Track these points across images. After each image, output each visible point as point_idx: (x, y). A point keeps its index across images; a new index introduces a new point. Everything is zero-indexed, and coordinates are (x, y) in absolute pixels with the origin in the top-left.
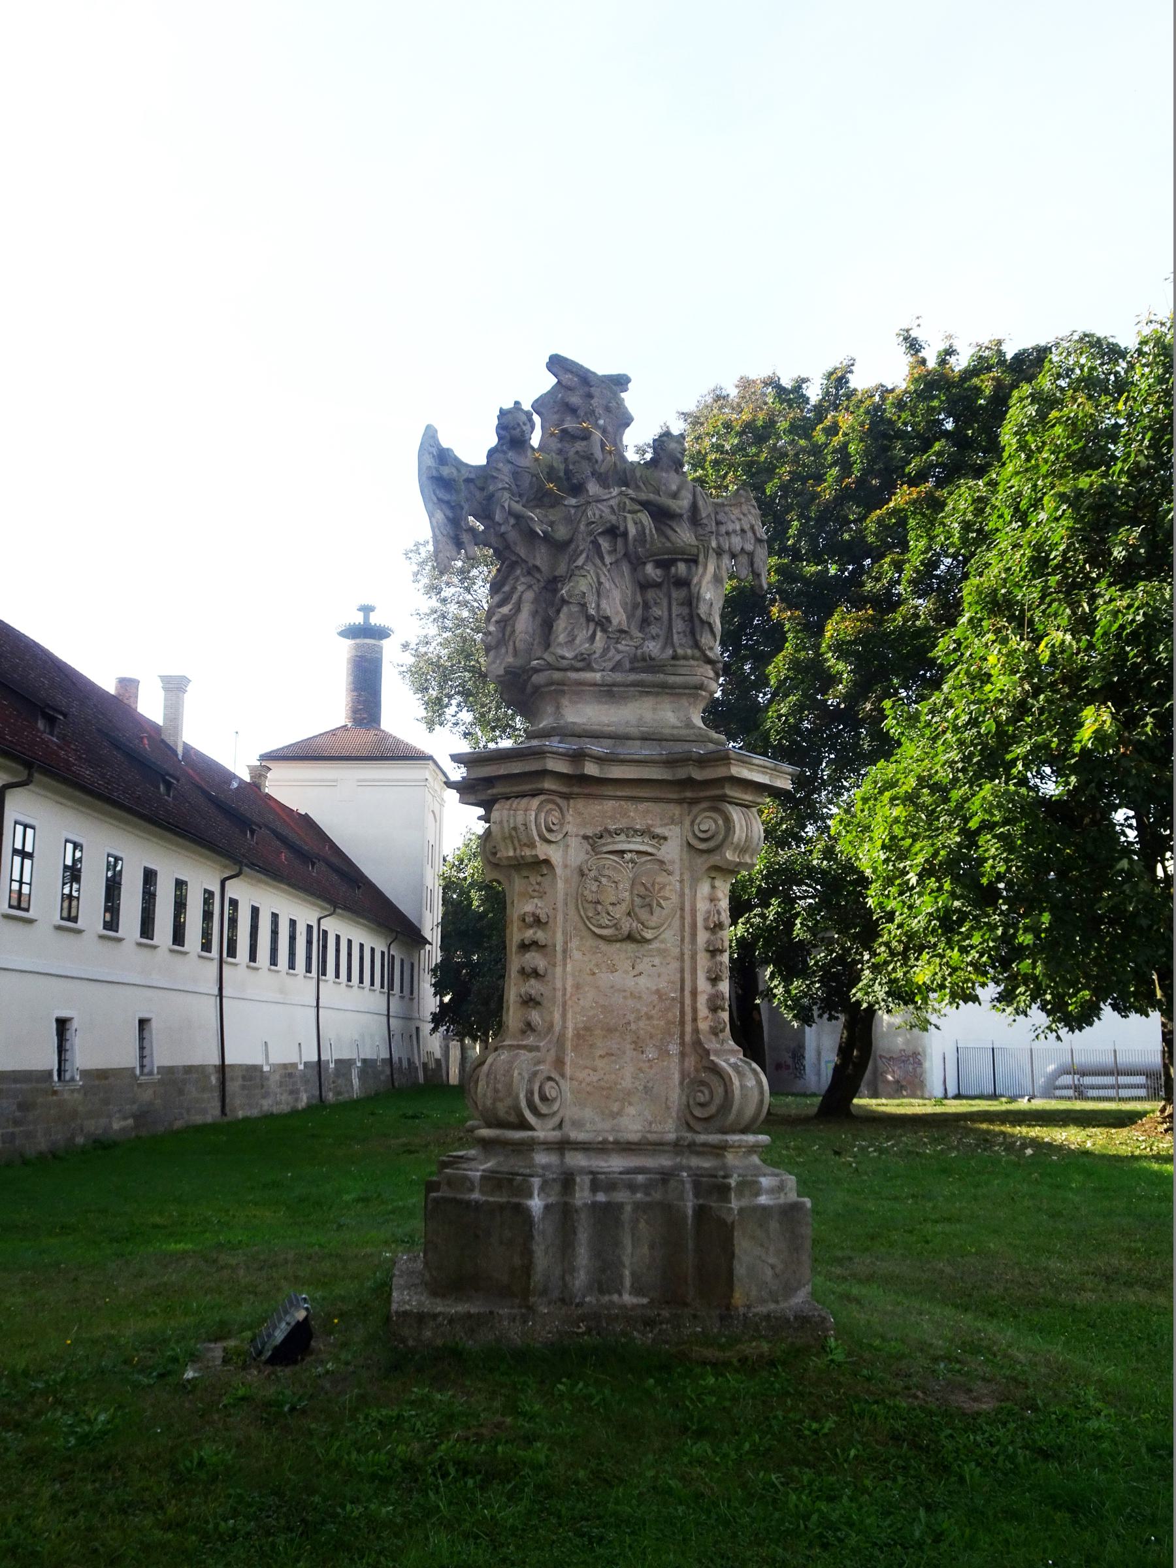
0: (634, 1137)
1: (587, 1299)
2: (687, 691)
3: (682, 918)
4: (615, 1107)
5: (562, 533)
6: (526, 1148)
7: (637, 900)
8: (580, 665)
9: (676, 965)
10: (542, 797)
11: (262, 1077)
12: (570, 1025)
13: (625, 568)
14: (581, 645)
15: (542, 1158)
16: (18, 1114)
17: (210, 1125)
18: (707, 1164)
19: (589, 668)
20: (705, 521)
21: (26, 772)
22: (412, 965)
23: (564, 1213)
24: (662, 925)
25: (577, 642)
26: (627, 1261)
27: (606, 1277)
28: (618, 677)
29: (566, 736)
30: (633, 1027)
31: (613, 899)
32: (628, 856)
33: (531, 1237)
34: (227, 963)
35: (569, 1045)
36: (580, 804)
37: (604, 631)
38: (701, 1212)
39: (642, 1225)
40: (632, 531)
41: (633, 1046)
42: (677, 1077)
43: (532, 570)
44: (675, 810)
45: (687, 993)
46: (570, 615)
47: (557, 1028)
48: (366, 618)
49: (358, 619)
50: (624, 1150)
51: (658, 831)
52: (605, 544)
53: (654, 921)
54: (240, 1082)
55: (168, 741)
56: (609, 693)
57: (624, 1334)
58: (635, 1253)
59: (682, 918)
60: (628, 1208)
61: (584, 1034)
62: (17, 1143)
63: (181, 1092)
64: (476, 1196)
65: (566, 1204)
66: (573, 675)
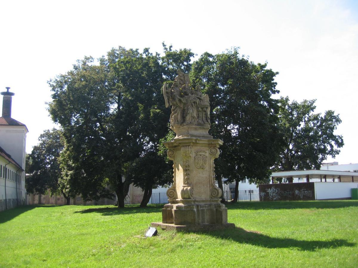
9: (208, 173)
18: (215, 203)
22: (20, 176)
30: (203, 182)
38: (216, 210)
42: (209, 190)
43: (180, 108)
48: (8, 90)
49: (6, 90)
52: (193, 104)
58: (207, 217)
60: (205, 210)
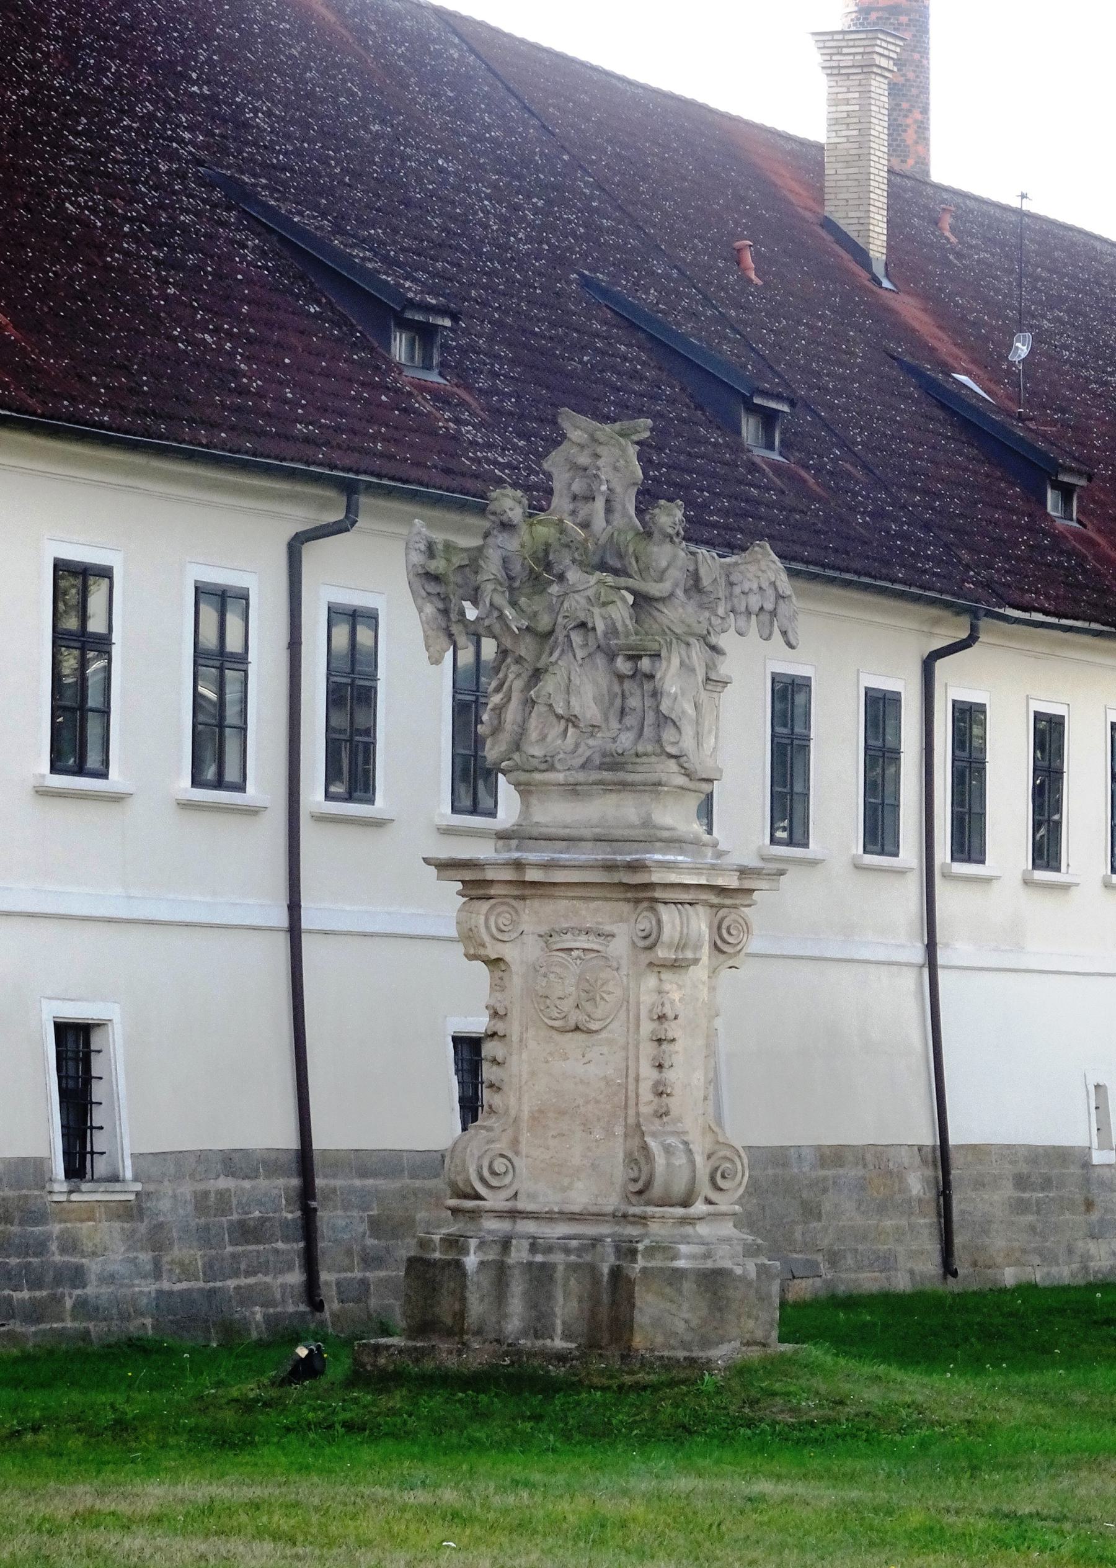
0: (576, 1209)
1: (522, 1342)
2: (647, 788)
3: (628, 1010)
4: (566, 1182)
5: (544, 623)
6: (474, 1215)
7: (583, 995)
8: (543, 766)
10: (492, 901)
11: (1087, 1181)
12: (526, 1109)
13: (600, 660)
14: (553, 742)
15: (491, 1224)
16: (370, 1242)
17: (900, 1297)
19: (552, 768)
20: (709, 589)
21: (344, 499)
23: (500, 1272)
24: (608, 1017)
25: (549, 738)
26: (558, 1311)
27: (539, 1326)
28: (581, 777)
29: (524, 838)
31: (561, 994)
32: (575, 953)
33: (464, 1287)
34: (947, 876)
35: (524, 1126)
36: (536, 903)
37: (575, 726)
39: (572, 1282)
40: (600, 627)
41: (582, 1127)
43: (519, 660)
44: (626, 908)
45: (631, 1080)
46: (539, 715)
47: (513, 1113)
50: (570, 1219)
51: (608, 928)
53: (599, 1013)
54: (1008, 1191)
55: (842, 223)
56: (573, 790)
57: (541, 1367)
58: (566, 1307)
59: (628, 1010)
60: (561, 1268)
61: (538, 1117)
62: (373, 1302)
63: (811, 1211)
64: (437, 1255)
65: (502, 1262)
66: (538, 776)
